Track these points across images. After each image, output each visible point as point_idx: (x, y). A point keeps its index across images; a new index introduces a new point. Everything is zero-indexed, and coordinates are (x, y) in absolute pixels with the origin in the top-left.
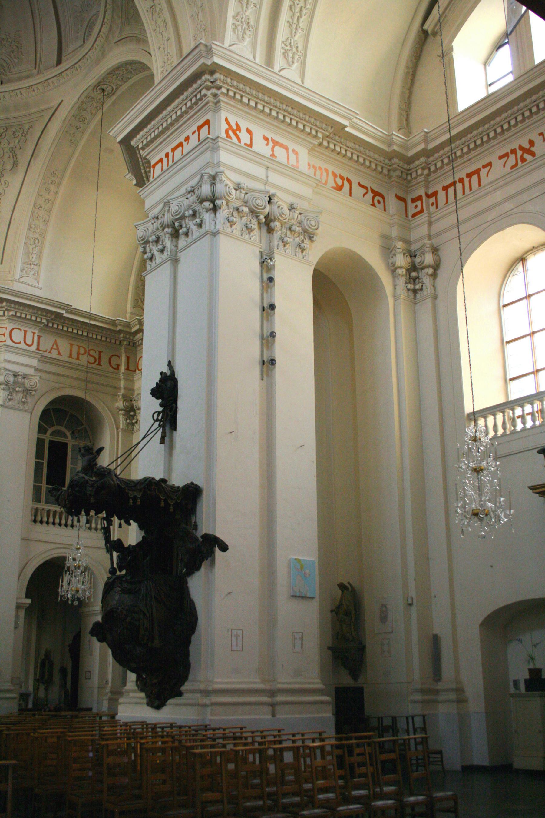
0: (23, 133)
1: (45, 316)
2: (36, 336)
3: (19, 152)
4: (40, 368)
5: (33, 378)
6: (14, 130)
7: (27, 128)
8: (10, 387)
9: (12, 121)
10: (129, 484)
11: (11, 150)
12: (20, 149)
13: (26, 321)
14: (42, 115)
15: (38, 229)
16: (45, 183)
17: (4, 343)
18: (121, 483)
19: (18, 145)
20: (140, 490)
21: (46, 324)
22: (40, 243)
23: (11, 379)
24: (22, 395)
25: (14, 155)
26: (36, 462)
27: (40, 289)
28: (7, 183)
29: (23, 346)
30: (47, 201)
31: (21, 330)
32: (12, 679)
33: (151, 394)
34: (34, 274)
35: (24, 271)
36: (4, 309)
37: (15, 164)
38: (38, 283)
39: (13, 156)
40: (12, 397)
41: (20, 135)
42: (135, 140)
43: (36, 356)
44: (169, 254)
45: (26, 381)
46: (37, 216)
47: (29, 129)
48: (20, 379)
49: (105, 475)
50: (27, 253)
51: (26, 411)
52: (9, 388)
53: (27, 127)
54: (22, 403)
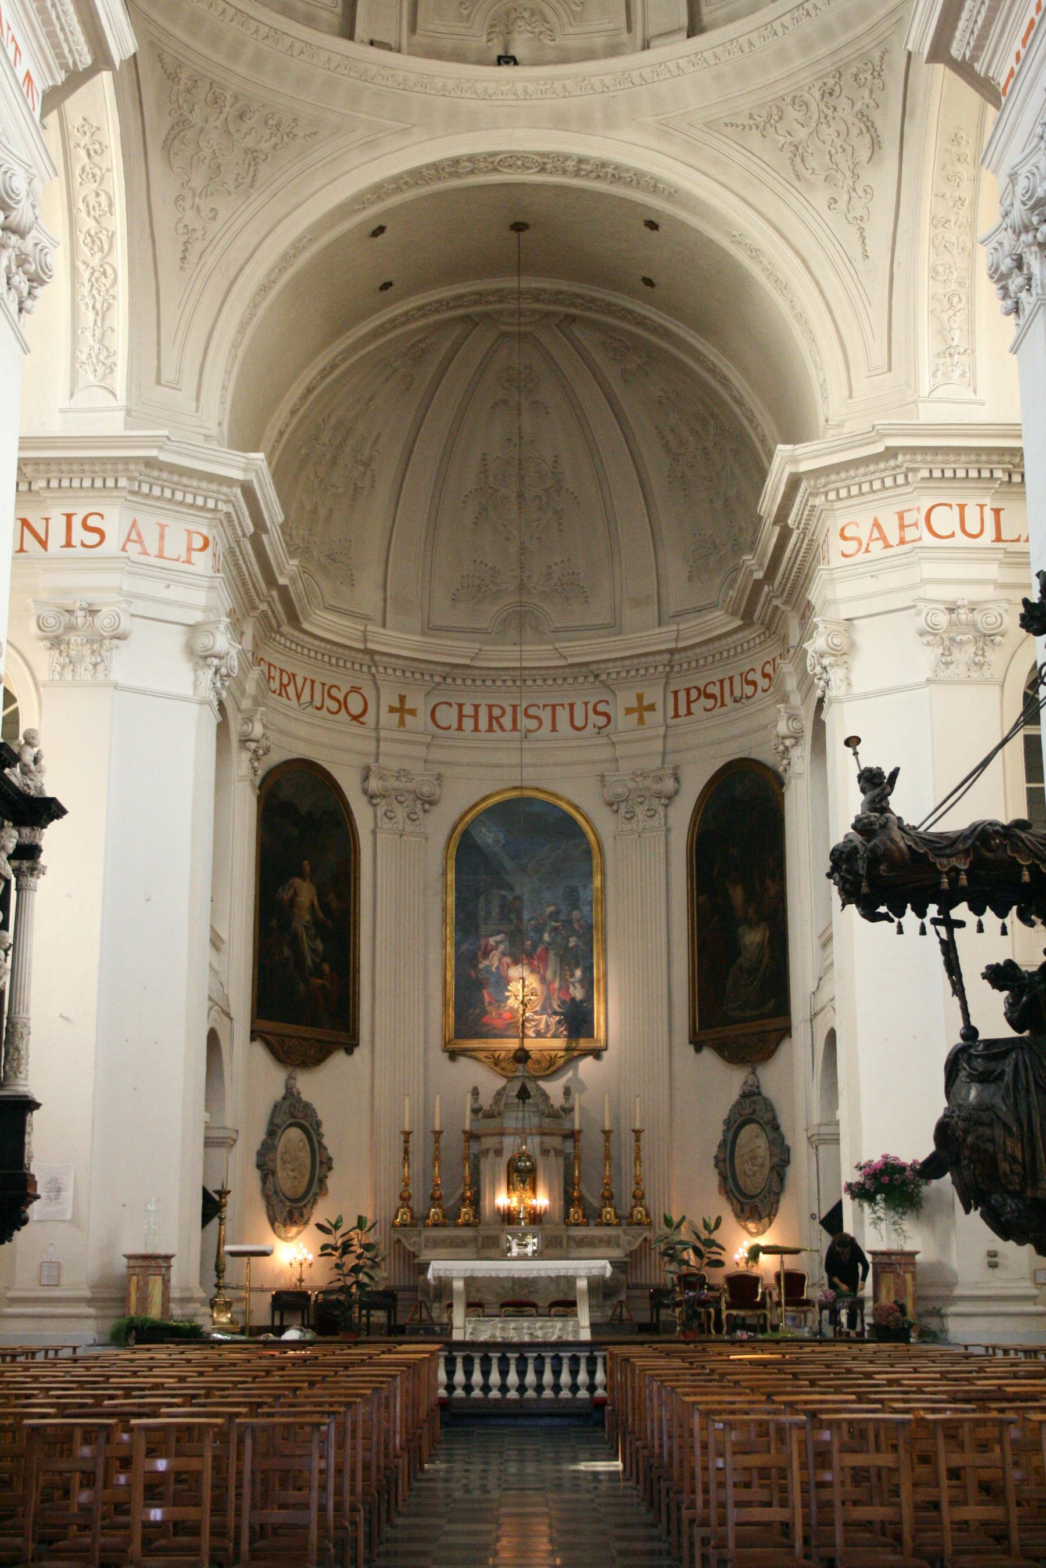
0: (874, 70)
1: (999, 463)
2: (987, 511)
3: (877, 116)
4: (1009, 580)
5: (991, 606)
6: (854, 70)
7: (878, 58)
8: (945, 636)
9: (846, 52)
10: (938, 843)
11: (860, 116)
12: (878, 107)
13: (957, 485)
14: (898, 17)
15: (953, 270)
16: (944, 166)
17: (918, 544)
18: (916, 843)
19: (871, 101)
20: (966, 852)
21: (1006, 479)
22: (964, 301)
23: (943, 619)
24: (973, 650)
25: (869, 124)
26: (1029, 790)
27: (983, 405)
28: (869, 190)
29: (961, 540)
30: (959, 204)
31: (950, 506)
32: (1034, 1272)
33: (1022, 626)
34: (963, 375)
35: (939, 374)
36: (903, 470)
37: (876, 144)
38: (975, 391)
39: (867, 128)
40: (949, 659)
41: (870, 77)
42: (955, 44)
43: (993, 556)
44: (1040, 291)
45: (977, 616)
46: (944, 243)
47: (882, 58)
48: (963, 615)
49: (875, 830)
50: (942, 332)
51: (985, 682)
52: (942, 639)
53: (876, 55)
54: (976, 668)
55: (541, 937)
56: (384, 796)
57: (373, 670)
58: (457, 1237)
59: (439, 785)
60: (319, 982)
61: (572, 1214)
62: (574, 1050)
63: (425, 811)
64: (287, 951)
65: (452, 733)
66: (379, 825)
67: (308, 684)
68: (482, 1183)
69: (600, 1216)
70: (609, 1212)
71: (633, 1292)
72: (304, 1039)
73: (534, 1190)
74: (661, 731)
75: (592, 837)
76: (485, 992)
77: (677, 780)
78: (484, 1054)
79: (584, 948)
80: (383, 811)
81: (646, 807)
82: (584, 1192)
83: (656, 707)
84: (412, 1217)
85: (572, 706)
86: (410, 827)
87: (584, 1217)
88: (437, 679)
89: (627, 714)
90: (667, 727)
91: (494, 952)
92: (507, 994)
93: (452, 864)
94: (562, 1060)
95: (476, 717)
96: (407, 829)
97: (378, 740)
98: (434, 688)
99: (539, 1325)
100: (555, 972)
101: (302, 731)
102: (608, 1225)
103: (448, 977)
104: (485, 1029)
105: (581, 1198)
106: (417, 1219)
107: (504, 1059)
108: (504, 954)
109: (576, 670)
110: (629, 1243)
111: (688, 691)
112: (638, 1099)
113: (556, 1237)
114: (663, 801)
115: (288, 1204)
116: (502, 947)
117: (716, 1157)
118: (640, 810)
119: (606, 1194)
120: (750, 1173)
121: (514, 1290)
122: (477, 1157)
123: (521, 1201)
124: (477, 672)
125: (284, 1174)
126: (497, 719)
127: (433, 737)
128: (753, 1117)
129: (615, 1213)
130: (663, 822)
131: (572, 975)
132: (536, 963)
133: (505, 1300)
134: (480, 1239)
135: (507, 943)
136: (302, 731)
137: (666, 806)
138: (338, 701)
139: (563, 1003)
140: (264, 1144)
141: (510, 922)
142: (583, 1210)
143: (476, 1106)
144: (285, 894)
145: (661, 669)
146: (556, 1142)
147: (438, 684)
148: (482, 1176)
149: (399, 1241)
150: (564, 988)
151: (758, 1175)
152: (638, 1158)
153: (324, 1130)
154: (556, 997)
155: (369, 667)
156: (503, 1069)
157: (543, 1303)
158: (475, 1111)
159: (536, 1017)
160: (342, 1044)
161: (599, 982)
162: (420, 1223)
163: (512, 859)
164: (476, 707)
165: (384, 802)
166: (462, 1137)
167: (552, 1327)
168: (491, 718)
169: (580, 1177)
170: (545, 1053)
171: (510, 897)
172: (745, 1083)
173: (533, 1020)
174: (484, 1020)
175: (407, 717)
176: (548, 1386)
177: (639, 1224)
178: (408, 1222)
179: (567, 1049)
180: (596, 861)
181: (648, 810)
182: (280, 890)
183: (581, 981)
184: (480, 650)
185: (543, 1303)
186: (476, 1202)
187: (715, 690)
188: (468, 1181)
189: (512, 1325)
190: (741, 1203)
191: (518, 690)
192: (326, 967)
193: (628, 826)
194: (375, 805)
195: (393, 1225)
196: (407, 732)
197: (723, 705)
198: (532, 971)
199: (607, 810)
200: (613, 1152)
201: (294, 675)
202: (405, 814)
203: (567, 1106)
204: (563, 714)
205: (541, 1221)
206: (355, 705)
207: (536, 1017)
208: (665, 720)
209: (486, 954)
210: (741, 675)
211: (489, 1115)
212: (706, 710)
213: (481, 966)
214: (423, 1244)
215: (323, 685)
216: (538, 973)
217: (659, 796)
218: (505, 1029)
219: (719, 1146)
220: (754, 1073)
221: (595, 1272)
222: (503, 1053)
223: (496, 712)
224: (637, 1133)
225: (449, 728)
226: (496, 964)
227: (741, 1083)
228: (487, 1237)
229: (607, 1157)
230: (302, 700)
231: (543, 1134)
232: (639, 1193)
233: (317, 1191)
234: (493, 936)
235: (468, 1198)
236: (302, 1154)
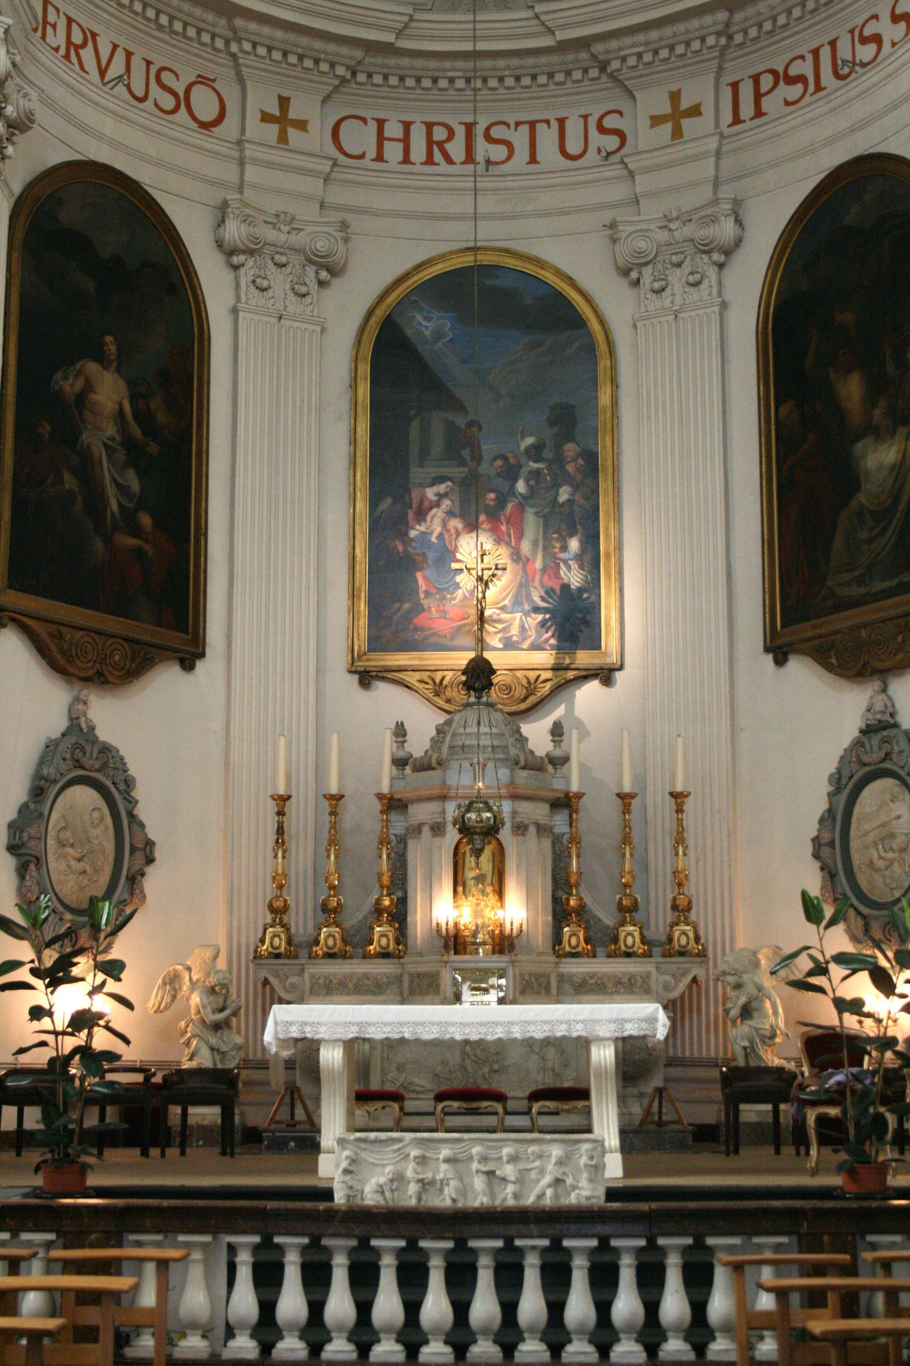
55: (513, 487)
56: (251, 252)
57: (234, 48)
58: (366, 976)
59: (346, 240)
60: (132, 542)
61: (566, 938)
62: (567, 668)
63: (321, 284)
64: (69, 481)
65: (366, 162)
66: (243, 299)
67: (120, 57)
68: (410, 883)
69: (615, 940)
70: (629, 934)
71: (679, 1072)
72: (100, 633)
73: (500, 893)
74: (712, 144)
75: (594, 325)
76: (419, 575)
77: (739, 222)
78: (418, 675)
79: (583, 502)
80: (250, 278)
81: (687, 271)
82: (588, 900)
83: (703, 109)
84: (289, 942)
85: (562, 122)
86: (294, 306)
87: (587, 941)
88: (340, 71)
89: (652, 126)
90: (722, 136)
91: (434, 511)
92: (455, 566)
93: (365, 369)
94: (548, 685)
95: (406, 140)
96: (291, 309)
97: (242, 163)
98: (336, 88)
99: (506, 1151)
100: (535, 544)
101: (108, 126)
102: (628, 955)
103: (358, 552)
104: (419, 636)
105: (581, 910)
106: (300, 946)
107: (451, 684)
108: (450, 514)
109: (570, 57)
111: (756, 79)
112: (680, 740)
113: (537, 976)
114: (716, 256)
115: (68, 916)
116: (446, 503)
117: (816, 841)
118: (677, 278)
119: (626, 902)
120: (881, 864)
121: (463, 1067)
122: (403, 840)
123: (477, 913)
124: (406, 61)
125: (63, 866)
126: (440, 144)
127: (335, 164)
128: (887, 765)
129: (641, 934)
130: (715, 291)
131: (564, 548)
132: (504, 528)
133: (443, 1088)
134: (406, 979)
135: (456, 497)
136: (108, 126)
137: (721, 266)
138: (175, 95)
139: (549, 592)
140: (23, 810)
141: (462, 463)
142: (587, 930)
143: (401, 754)
145: (711, 41)
146: (538, 812)
147: (343, 80)
148: (410, 871)
149: (266, 982)
150: (552, 567)
151: (896, 867)
152: (680, 839)
153: (138, 793)
154: (537, 583)
155: (227, 43)
156: (448, 701)
157: (517, 1092)
158: (400, 763)
159: (504, 616)
160: (175, 651)
161: (608, 556)
162: (304, 953)
163: (464, 361)
164: (407, 126)
165: (251, 262)
166: (377, 806)
167: (540, 1157)
168: (430, 142)
169: (580, 873)
170: (519, 674)
171: (460, 421)
173: (499, 621)
174: (420, 620)
175: (292, 132)
176: (532, 1330)
177: (682, 954)
178: (282, 950)
179: (556, 668)
180: (604, 363)
181: (692, 273)
182: (59, 375)
183: (579, 558)
184: (411, 19)
185: (517, 1092)
187: (805, 68)
188: (386, 879)
189: (445, 1152)
190: (864, 917)
191: (472, 93)
192: (146, 520)
193: (654, 304)
194: (236, 268)
195: (257, 956)
196: (290, 151)
197: (819, 88)
198: (498, 541)
199: (623, 282)
200: (636, 835)
201: (94, 35)
202: (288, 286)
203: (558, 753)
204: (547, 137)
205: (512, 947)
206: (205, 107)
207: (504, 616)
208: (717, 126)
209: (421, 515)
210: (852, 32)
211: (423, 766)
212: (787, 103)
213: (413, 534)
214: (307, 988)
215: (149, 63)
216: (508, 544)
217: (706, 248)
218: (453, 637)
219: (821, 821)
220: (884, 690)
221: (631, 1030)
222: (449, 675)
223: (440, 134)
224: (678, 798)
225: (362, 156)
226: (438, 530)
228: (419, 975)
229: (626, 839)
230: (110, 75)
231: (514, 797)
232: (682, 901)
233: (126, 896)
234: (432, 485)
235: (386, 909)
236: (97, 832)
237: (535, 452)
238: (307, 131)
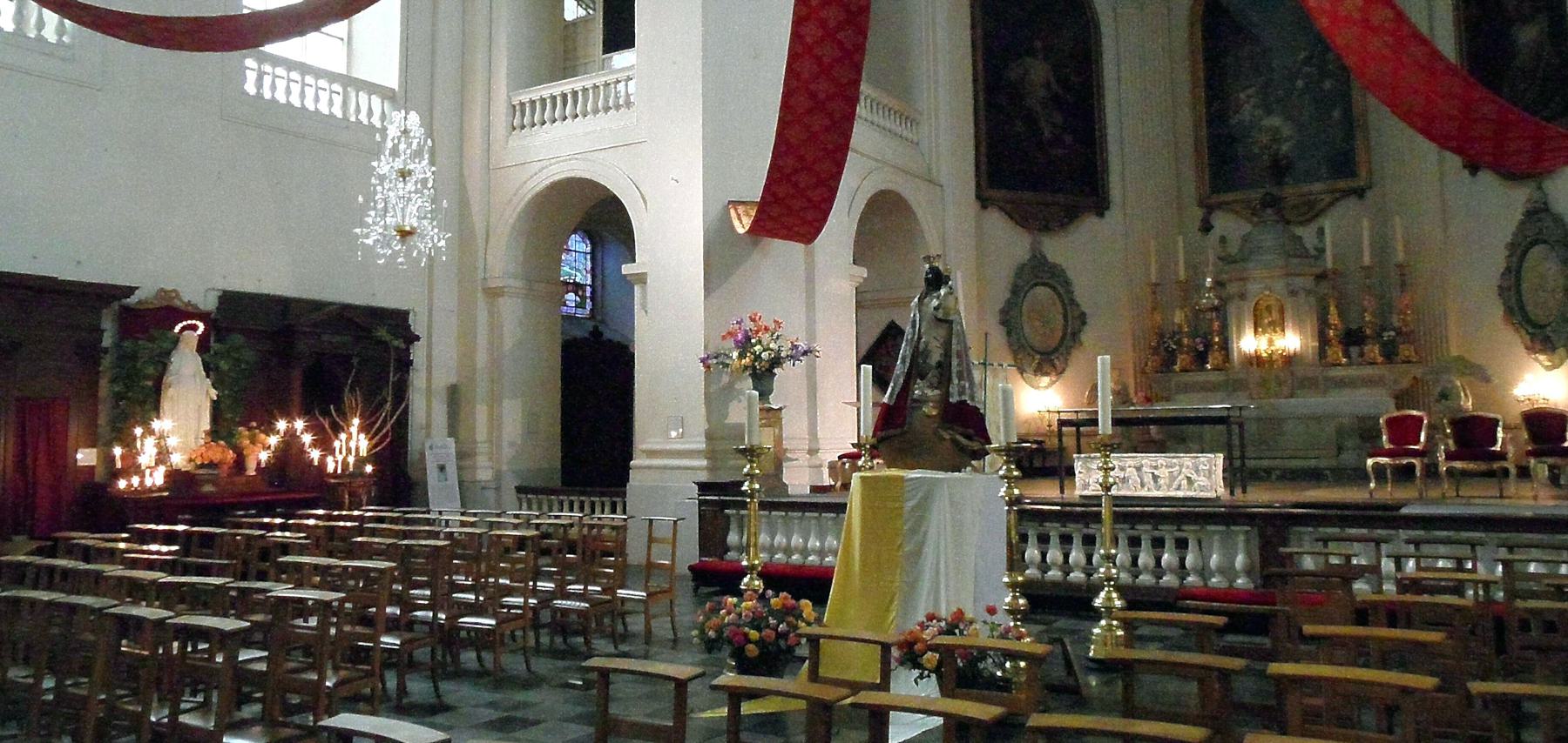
93: (1199, 27)
102: (1373, 363)
110: (1395, 382)
128: (1540, 237)
140: (1008, 302)
144: (1013, 74)
172: (1529, 201)
186: (1225, 347)
192: (1068, 139)
220: (1540, 188)
227: (1525, 200)
237: (1307, 61)
238: (697, 484)
